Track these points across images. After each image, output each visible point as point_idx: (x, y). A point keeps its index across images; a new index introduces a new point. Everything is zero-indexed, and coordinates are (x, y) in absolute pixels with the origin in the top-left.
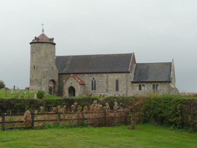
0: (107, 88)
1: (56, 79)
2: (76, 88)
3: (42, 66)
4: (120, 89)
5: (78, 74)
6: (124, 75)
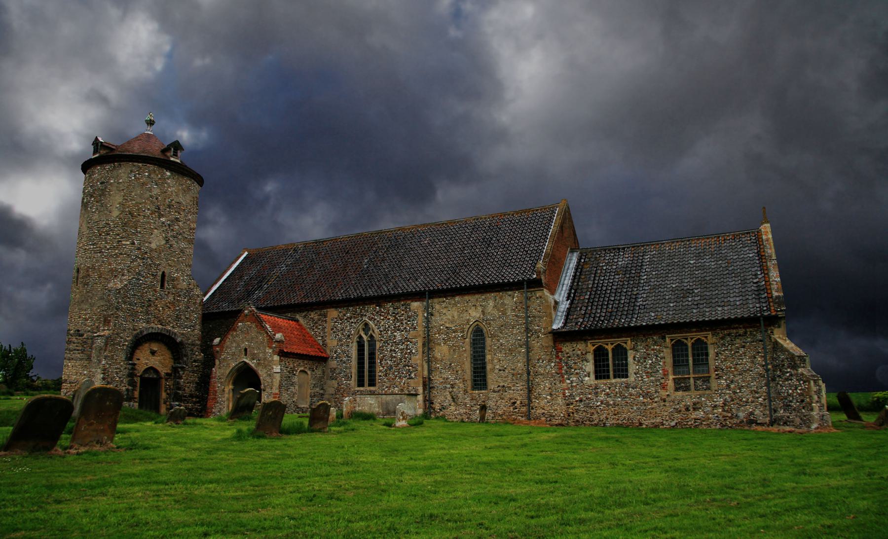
0: (426, 373)
1: (188, 330)
2: (262, 373)
3: (105, 269)
4: (493, 379)
5: (301, 311)
6: (511, 299)
